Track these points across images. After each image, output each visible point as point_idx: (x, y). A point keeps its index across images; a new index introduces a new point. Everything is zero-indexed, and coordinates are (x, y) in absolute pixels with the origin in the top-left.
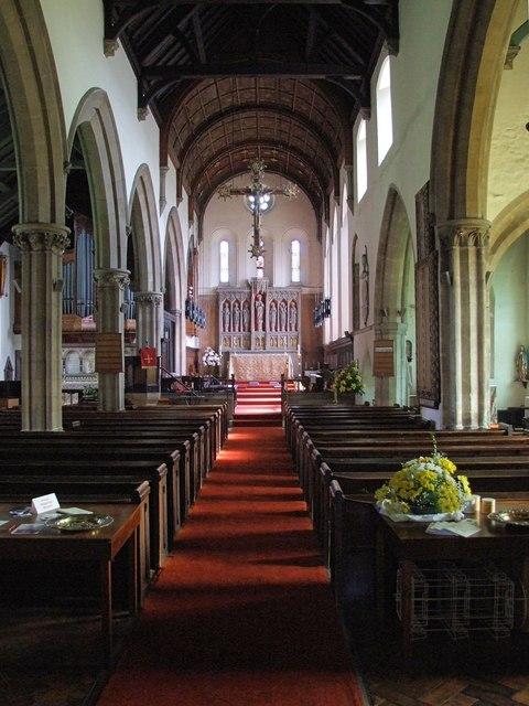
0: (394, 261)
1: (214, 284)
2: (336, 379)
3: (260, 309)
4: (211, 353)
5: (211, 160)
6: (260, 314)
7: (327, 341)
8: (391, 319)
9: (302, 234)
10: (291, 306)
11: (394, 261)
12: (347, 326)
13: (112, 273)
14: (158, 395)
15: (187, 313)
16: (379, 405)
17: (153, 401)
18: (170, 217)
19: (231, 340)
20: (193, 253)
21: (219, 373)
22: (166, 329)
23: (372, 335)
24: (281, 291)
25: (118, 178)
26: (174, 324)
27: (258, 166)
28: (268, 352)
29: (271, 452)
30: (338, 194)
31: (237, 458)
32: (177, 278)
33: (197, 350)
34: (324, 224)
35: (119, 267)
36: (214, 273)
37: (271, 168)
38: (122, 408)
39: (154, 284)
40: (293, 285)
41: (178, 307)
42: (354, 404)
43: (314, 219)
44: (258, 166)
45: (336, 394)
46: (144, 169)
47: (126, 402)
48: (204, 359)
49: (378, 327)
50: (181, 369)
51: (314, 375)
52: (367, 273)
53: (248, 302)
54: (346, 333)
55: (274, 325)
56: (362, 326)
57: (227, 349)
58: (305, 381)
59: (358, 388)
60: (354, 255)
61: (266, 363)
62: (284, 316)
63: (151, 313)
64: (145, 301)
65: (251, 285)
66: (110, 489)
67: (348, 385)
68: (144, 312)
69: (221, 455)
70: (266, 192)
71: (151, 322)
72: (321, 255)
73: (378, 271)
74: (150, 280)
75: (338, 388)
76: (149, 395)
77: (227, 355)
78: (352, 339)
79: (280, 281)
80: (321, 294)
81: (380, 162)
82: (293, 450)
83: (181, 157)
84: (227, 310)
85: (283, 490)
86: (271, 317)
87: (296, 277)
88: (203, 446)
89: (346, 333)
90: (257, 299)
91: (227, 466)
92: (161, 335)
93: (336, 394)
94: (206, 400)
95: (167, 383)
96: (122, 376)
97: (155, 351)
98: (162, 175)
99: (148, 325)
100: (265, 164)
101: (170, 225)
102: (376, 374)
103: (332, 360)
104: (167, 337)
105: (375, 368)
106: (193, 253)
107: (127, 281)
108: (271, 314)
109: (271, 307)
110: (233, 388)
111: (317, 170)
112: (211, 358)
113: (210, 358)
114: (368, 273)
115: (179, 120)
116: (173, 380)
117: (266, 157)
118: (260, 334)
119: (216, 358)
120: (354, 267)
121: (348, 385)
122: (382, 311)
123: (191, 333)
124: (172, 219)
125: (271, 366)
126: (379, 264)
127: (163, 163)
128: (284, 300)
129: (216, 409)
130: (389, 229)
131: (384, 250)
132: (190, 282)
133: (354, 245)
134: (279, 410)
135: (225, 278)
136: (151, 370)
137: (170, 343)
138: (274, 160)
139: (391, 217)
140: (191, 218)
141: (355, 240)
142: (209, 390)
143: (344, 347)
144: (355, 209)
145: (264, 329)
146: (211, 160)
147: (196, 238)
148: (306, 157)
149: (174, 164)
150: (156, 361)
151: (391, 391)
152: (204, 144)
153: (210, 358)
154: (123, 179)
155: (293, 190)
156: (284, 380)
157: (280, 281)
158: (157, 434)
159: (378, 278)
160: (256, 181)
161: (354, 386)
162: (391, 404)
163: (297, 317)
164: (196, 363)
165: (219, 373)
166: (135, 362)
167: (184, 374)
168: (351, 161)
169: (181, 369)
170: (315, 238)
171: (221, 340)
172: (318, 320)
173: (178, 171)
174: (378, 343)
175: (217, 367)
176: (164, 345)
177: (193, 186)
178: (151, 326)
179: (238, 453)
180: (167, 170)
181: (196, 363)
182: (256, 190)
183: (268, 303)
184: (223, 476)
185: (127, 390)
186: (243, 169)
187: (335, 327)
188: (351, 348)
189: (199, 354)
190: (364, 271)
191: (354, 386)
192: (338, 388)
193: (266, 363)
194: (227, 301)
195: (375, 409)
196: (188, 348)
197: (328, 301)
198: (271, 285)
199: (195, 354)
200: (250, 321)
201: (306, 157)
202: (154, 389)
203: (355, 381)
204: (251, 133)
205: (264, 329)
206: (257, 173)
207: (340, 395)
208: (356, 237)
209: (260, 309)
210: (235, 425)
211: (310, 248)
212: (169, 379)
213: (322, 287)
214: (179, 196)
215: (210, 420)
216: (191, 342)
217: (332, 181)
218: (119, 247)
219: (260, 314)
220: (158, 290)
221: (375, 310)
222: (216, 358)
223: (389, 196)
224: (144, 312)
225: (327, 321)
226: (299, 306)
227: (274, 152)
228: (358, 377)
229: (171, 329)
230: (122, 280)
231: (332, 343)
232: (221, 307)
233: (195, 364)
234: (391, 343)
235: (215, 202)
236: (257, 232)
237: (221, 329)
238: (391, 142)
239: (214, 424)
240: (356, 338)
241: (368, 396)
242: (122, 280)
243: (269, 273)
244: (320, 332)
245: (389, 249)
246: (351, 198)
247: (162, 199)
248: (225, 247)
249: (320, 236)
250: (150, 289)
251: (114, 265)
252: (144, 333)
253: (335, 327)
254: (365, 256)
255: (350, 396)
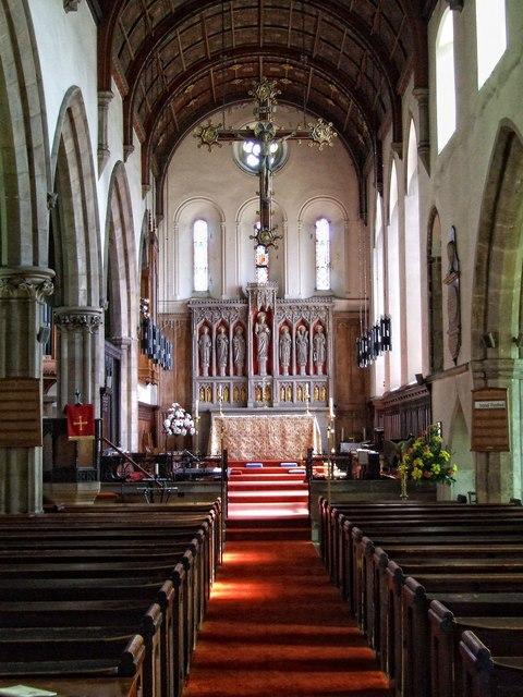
0: (507, 252)
1: (183, 294)
2: (406, 457)
3: (264, 336)
4: (180, 413)
5: (181, 79)
6: (263, 347)
7: (379, 390)
8: (502, 352)
9: (333, 209)
10: (315, 332)
11: (507, 252)
12: (418, 364)
13: (24, 274)
14: (97, 486)
15: (144, 344)
16: (482, 501)
17: (86, 497)
18: (114, 183)
19: (213, 392)
20: (149, 241)
21: (195, 445)
22: (107, 373)
23: (468, 381)
24: (297, 306)
25: (34, 112)
26: (118, 363)
27: (265, 92)
28: (278, 412)
29: (299, 584)
30: (399, 138)
31: (245, 594)
32: (122, 283)
33: (154, 409)
34: (372, 189)
35: (36, 263)
36: (183, 275)
37: (288, 97)
38: (39, 510)
39: (87, 295)
40: (317, 295)
41: (124, 334)
42: (434, 498)
43: (354, 183)
44: (265, 92)
45: (404, 483)
46: (74, 94)
47: (45, 501)
48: (168, 423)
49: (478, 366)
50: (130, 440)
51: (361, 451)
52: (456, 272)
53: (242, 325)
54: (419, 377)
55: (206, 366)
56: (448, 364)
57: (207, 405)
58: (344, 461)
59: (446, 472)
60: (430, 244)
61: (274, 429)
62: (304, 349)
63: (84, 344)
64: (71, 322)
65: (247, 296)
66: (79, 651)
67: (427, 467)
68: (71, 343)
69: (218, 590)
70: (279, 135)
71: (84, 360)
72: (367, 243)
73: (478, 269)
74: (83, 286)
75: (410, 471)
76: (81, 487)
77: (206, 415)
78: (430, 388)
79: (297, 289)
80: (369, 311)
81: (481, 82)
82: (348, 583)
83: (131, 76)
84: (207, 339)
85: (305, 652)
86: (282, 353)
87: (324, 283)
88: (196, 572)
89: (419, 377)
90: (257, 320)
91: (226, 609)
92: (101, 383)
93: (404, 483)
94: (181, 495)
95: (108, 467)
96: (38, 452)
97: (91, 409)
98: (102, 106)
99: (78, 365)
100: (277, 87)
101: (114, 198)
102: (476, 448)
103: (390, 426)
104: (109, 385)
105: (474, 437)
106: (149, 241)
107: (49, 288)
108: (281, 345)
109: (281, 333)
110: (224, 474)
111: (360, 97)
112: (180, 422)
113: (178, 423)
114: (459, 274)
115: (128, 14)
116: (121, 458)
117: (278, 77)
118: (264, 380)
119: (188, 422)
120: (431, 263)
121: (427, 467)
122: (487, 338)
123: (147, 378)
124: (117, 187)
125: (283, 436)
126: (479, 259)
127: (103, 87)
128: (303, 322)
129: (206, 510)
130: (497, 197)
131: (488, 233)
132: (145, 293)
133: (431, 226)
134: (304, 512)
135: (202, 284)
136: (84, 442)
137: (113, 396)
138: (237, 82)
139: (501, 177)
140: (145, 182)
141: (432, 218)
142: (181, 478)
143: (413, 402)
144: (435, 164)
145: (270, 371)
146: (181, 79)
147: (153, 217)
148: (339, 75)
149: (120, 88)
150: (92, 427)
151: (504, 476)
152: (168, 53)
153: (178, 423)
154: (43, 113)
155: (324, 134)
156: (309, 462)
157: (297, 289)
158: (94, 553)
159: (478, 282)
160: (263, 117)
161: (437, 468)
162: (505, 500)
163: (328, 349)
164: (153, 428)
165: (195, 445)
166: (58, 428)
167: (135, 449)
168: (425, 81)
169: (130, 440)
170: (354, 215)
171: (197, 387)
172: (366, 356)
173: (126, 99)
174: (480, 392)
175: (189, 436)
176: (106, 399)
177: (148, 127)
178: (84, 365)
179: (247, 586)
180: (111, 97)
181: (153, 428)
182: (262, 133)
183: (277, 325)
184: (224, 627)
185: (47, 478)
186: (241, 95)
187: (393, 371)
188: (427, 403)
189: (159, 415)
190: (452, 271)
191: (437, 468)
192: (410, 471)
193: (274, 429)
194: (206, 324)
195: (478, 508)
196: (141, 406)
197: (386, 322)
198: (280, 295)
199: (150, 413)
200: (245, 361)
201: (339, 75)
202: (88, 477)
203: (438, 459)
204: (248, 37)
205: (270, 371)
206: (264, 104)
207: (412, 488)
208: (434, 213)
209: (264, 336)
210: (230, 537)
211: (348, 232)
212: (114, 457)
213: (370, 299)
214: (127, 142)
215: (203, 528)
216: (145, 395)
217: (387, 118)
218: (35, 230)
219: (263, 347)
220: (95, 304)
221: (474, 337)
222: (188, 422)
223: (499, 139)
224: (71, 343)
225: (379, 361)
226: (330, 331)
227: (287, 67)
228: (444, 453)
229: (115, 369)
230: (40, 286)
231: (389, 395)
232: (196, 333)
233: (152, 430)
234: (502, 393)
235: (188, 151)
236: (264, 205)
237: (196, 373)
238: (504, 47)
239: (207, 534)
240: (436, 385)
241: (462, 483)
242: (40, 286)
243: (278, 279)
244: (366, 377)
245: (497, 233)
246: (426, 145)
247: (102, 148)
248: (201, 230)
249: (364, 212)
250: (82, 302)
251: (26, 260)
252: (71, 378)
253: (393, 371)
254: (453, 244)
255: (428, 485)
